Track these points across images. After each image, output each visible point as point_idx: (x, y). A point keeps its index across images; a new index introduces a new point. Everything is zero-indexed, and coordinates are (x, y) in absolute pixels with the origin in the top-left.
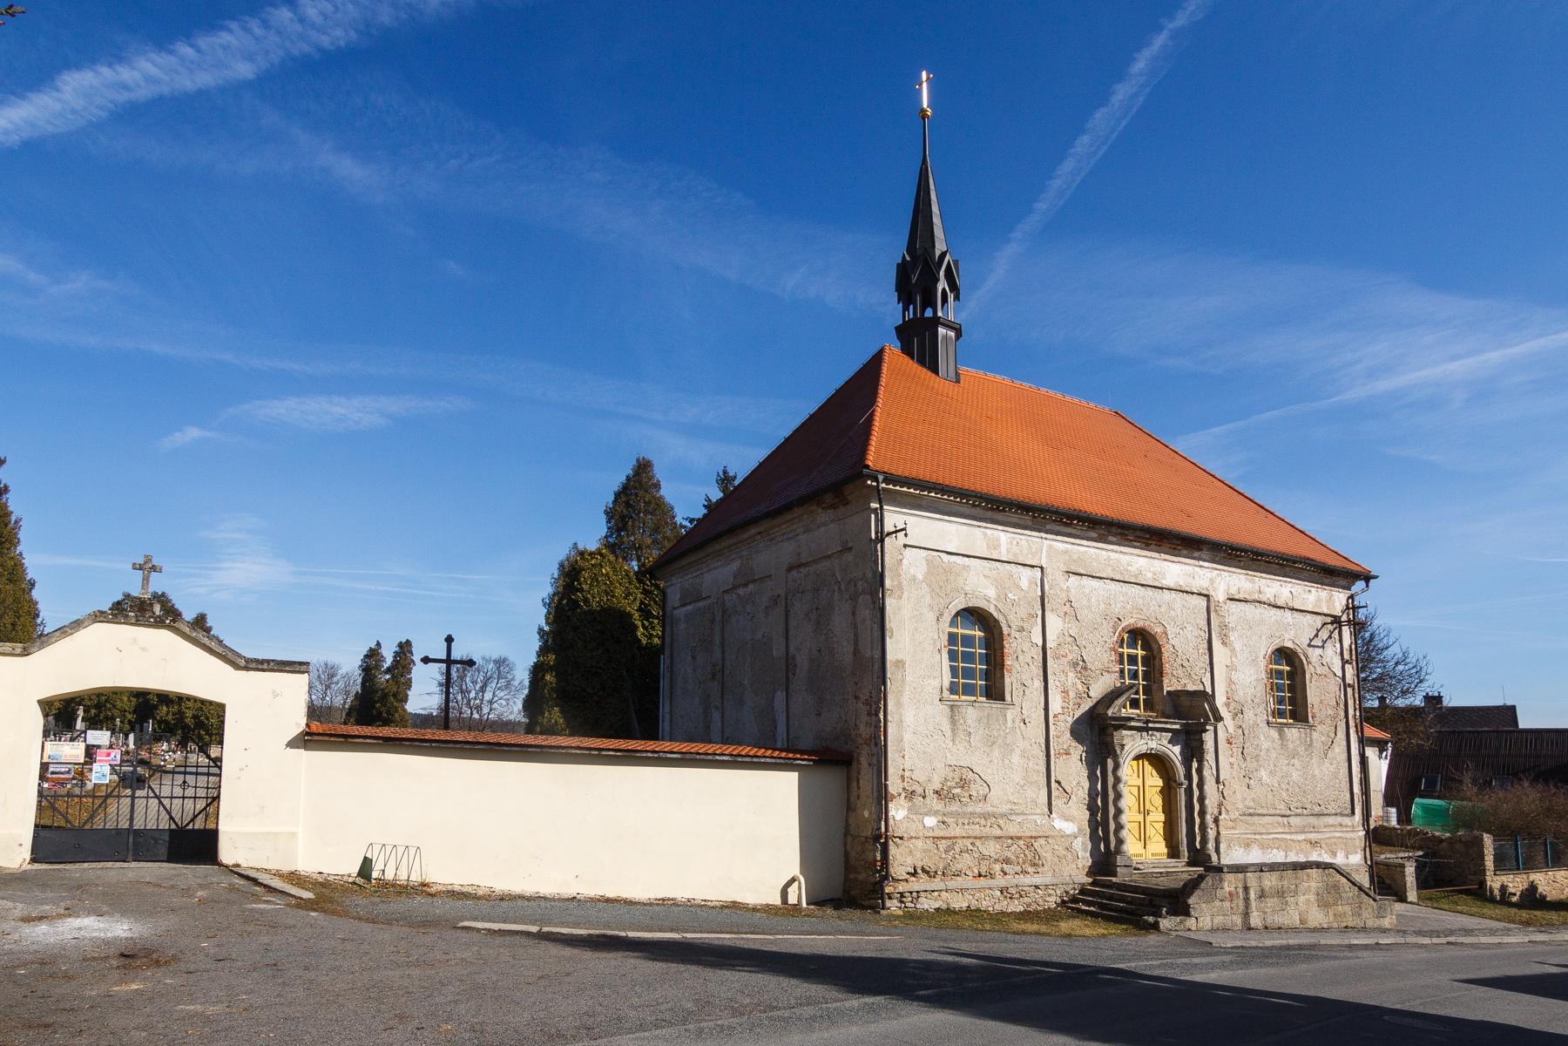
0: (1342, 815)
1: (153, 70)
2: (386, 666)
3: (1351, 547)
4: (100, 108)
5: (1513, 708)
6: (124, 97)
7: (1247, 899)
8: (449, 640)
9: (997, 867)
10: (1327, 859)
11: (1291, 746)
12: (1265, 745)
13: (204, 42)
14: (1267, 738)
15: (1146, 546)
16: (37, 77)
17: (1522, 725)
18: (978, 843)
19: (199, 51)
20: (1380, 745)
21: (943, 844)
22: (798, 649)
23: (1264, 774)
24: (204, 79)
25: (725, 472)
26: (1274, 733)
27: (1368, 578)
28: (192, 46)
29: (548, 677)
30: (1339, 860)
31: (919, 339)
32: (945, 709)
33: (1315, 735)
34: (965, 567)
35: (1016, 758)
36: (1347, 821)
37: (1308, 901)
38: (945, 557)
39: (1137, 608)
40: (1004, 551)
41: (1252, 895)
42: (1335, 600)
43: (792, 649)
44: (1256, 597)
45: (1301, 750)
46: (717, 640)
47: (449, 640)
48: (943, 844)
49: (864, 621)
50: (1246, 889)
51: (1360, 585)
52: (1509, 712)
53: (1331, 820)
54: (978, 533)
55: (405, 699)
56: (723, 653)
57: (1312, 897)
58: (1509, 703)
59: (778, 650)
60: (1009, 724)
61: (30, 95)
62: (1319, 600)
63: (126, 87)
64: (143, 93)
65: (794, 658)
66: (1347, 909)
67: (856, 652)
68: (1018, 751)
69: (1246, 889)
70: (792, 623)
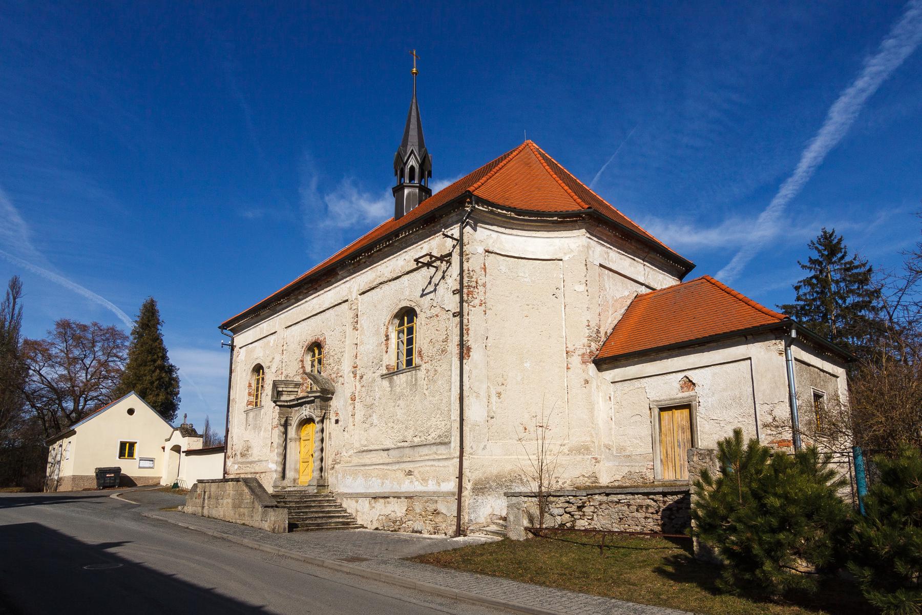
1: (873, 69)
4: (853, 113)
6: (864, 96)
8: (186, 416)
11: (398, 390)
13: (897, 31)
15: (274, 312)
16: (819, 120)
19: (895, 37)
24: (906, 51)
25: (825, 233)
28: (890, 38)
29: (803, 566)
36: (442, 449)
37: (228, 503)
39: (305, 333)
45: (407, 392)
47: (186, 416)
53: (425, 450)
57: (230, 501)
61: (820, 131)
63: (863, 90)
64: (873, 89)
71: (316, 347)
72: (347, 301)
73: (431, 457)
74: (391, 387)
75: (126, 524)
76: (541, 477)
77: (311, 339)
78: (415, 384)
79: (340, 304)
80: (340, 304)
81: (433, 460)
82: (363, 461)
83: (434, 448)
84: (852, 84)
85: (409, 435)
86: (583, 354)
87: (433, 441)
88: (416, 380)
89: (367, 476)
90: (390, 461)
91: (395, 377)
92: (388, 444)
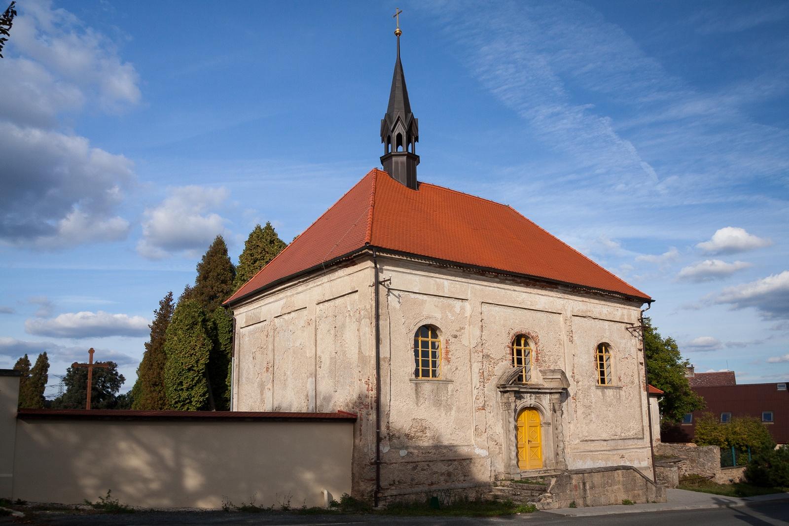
0: (638, 439)
2: (31, 368)
3: (646, 290)
5: (269, 227)
7: (585, 490)
9: (442, 478)
10: (628, 464)
12: (593, 401)
14: (596, 394)
15: (527, 285)
17: (737, 384)
18: (431, 464)
20: (658, 396)
21: (410, 467)
22: (323, 352)
23: (593, 415)
26: (599, 392)
27: (649, 301)
30: (636, 465)
31: (637, 299)
32: (413, 386)
33: (622, 393)
34: (423, 302)
35: (453, 412)
36: (640, 442)
38: (413, 295)
39: (521, 323)
40: (446, 291)
41: (588, 487)
42: (631, 313)
43: (319, 353)
44: (589, 314)
46: (270, 347)
48: (410, 467)
49: (365, 334)
50: (584, 484)
51: (646, 305)
52: (731, 376)
53: (630, 442)
54: (458, 285)
55: (43, 393)
56: (274, 355)
58: (731, 370)
59: (310, 353)
60: (450, 393)
62: (623, 315)
65: (320, 357)
66: (640, 492)
67: (360, 352)
68: (454, 408)
69: (584, 484)
70: (319, 336)
71: (520, 339)
72: (357, 291)
73: (634, 447)
74: (603, 396)
75: (511, 428)
76: (617, 504)
77: (518, 329)
78: (620, 398)
79: (555, 313)
80: (555, 313)
81: (637, 448)
82: (588, 448)
83: (636, 441)
84: (123, 314)
85: (619, 430)
86: (408, 500)
87: (633, 437)
88: (620, 395)
89: (593, 459)
90: (608, 448)
91: (606, 390)
92: (604, 436)
